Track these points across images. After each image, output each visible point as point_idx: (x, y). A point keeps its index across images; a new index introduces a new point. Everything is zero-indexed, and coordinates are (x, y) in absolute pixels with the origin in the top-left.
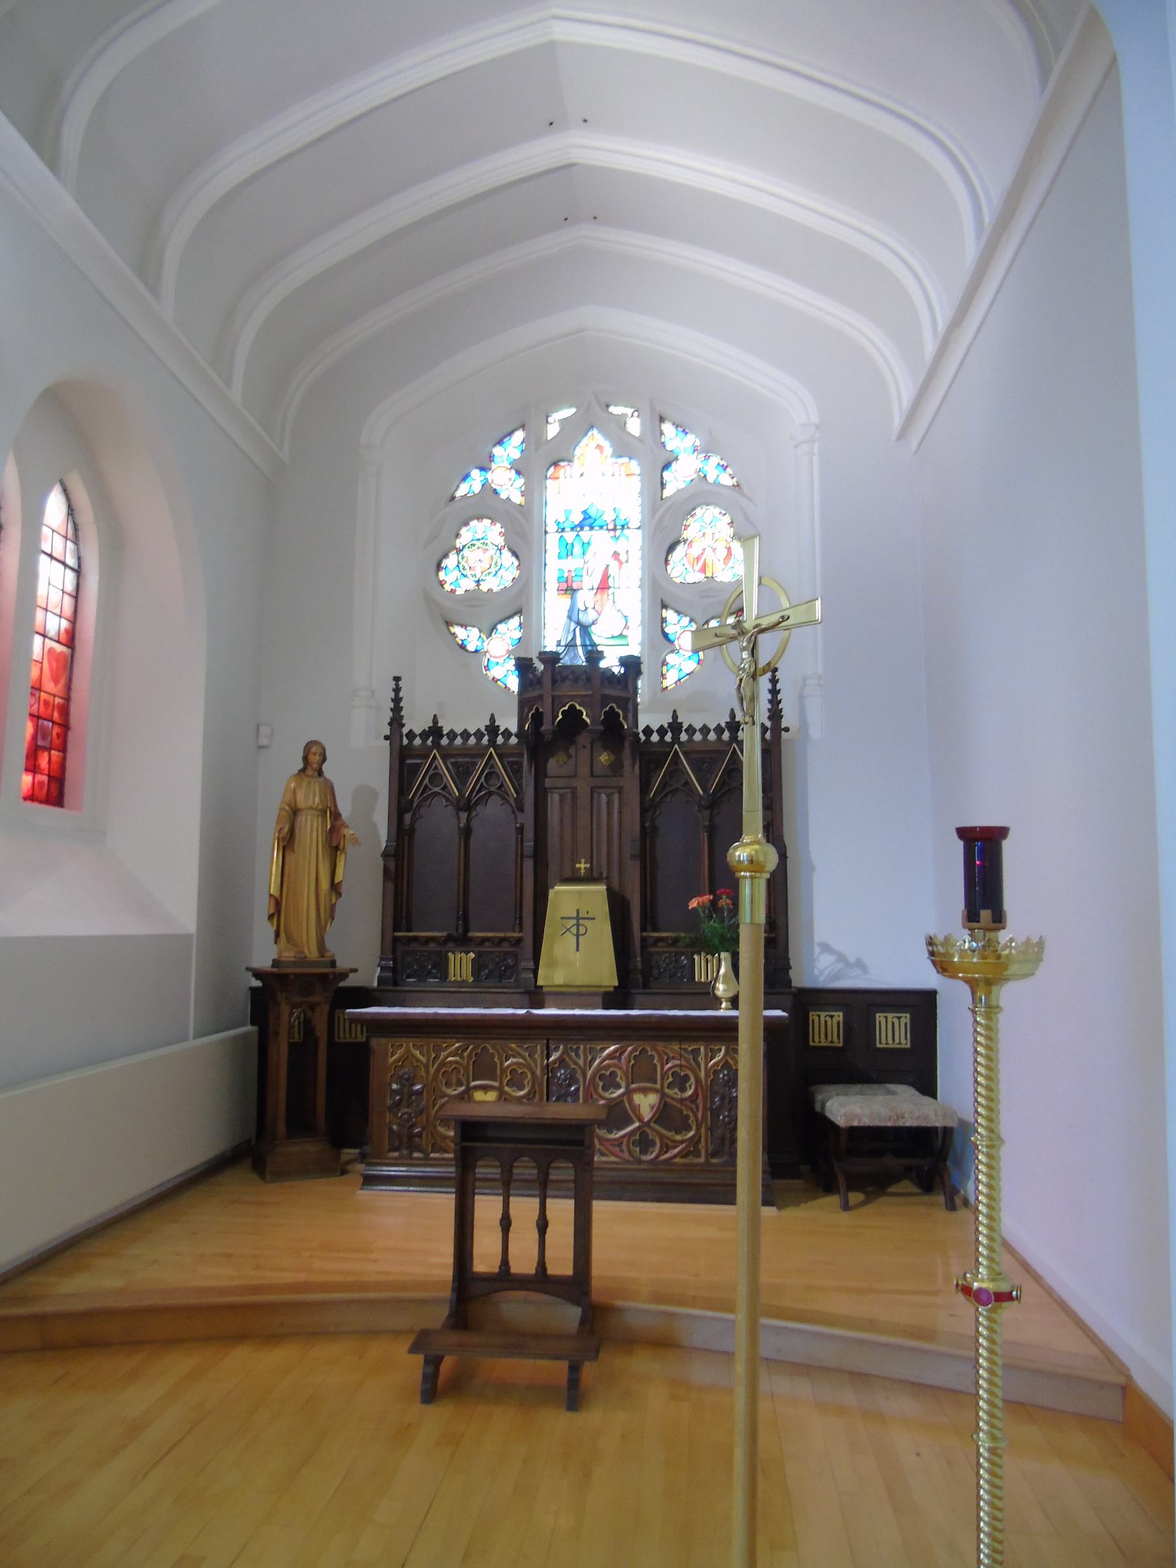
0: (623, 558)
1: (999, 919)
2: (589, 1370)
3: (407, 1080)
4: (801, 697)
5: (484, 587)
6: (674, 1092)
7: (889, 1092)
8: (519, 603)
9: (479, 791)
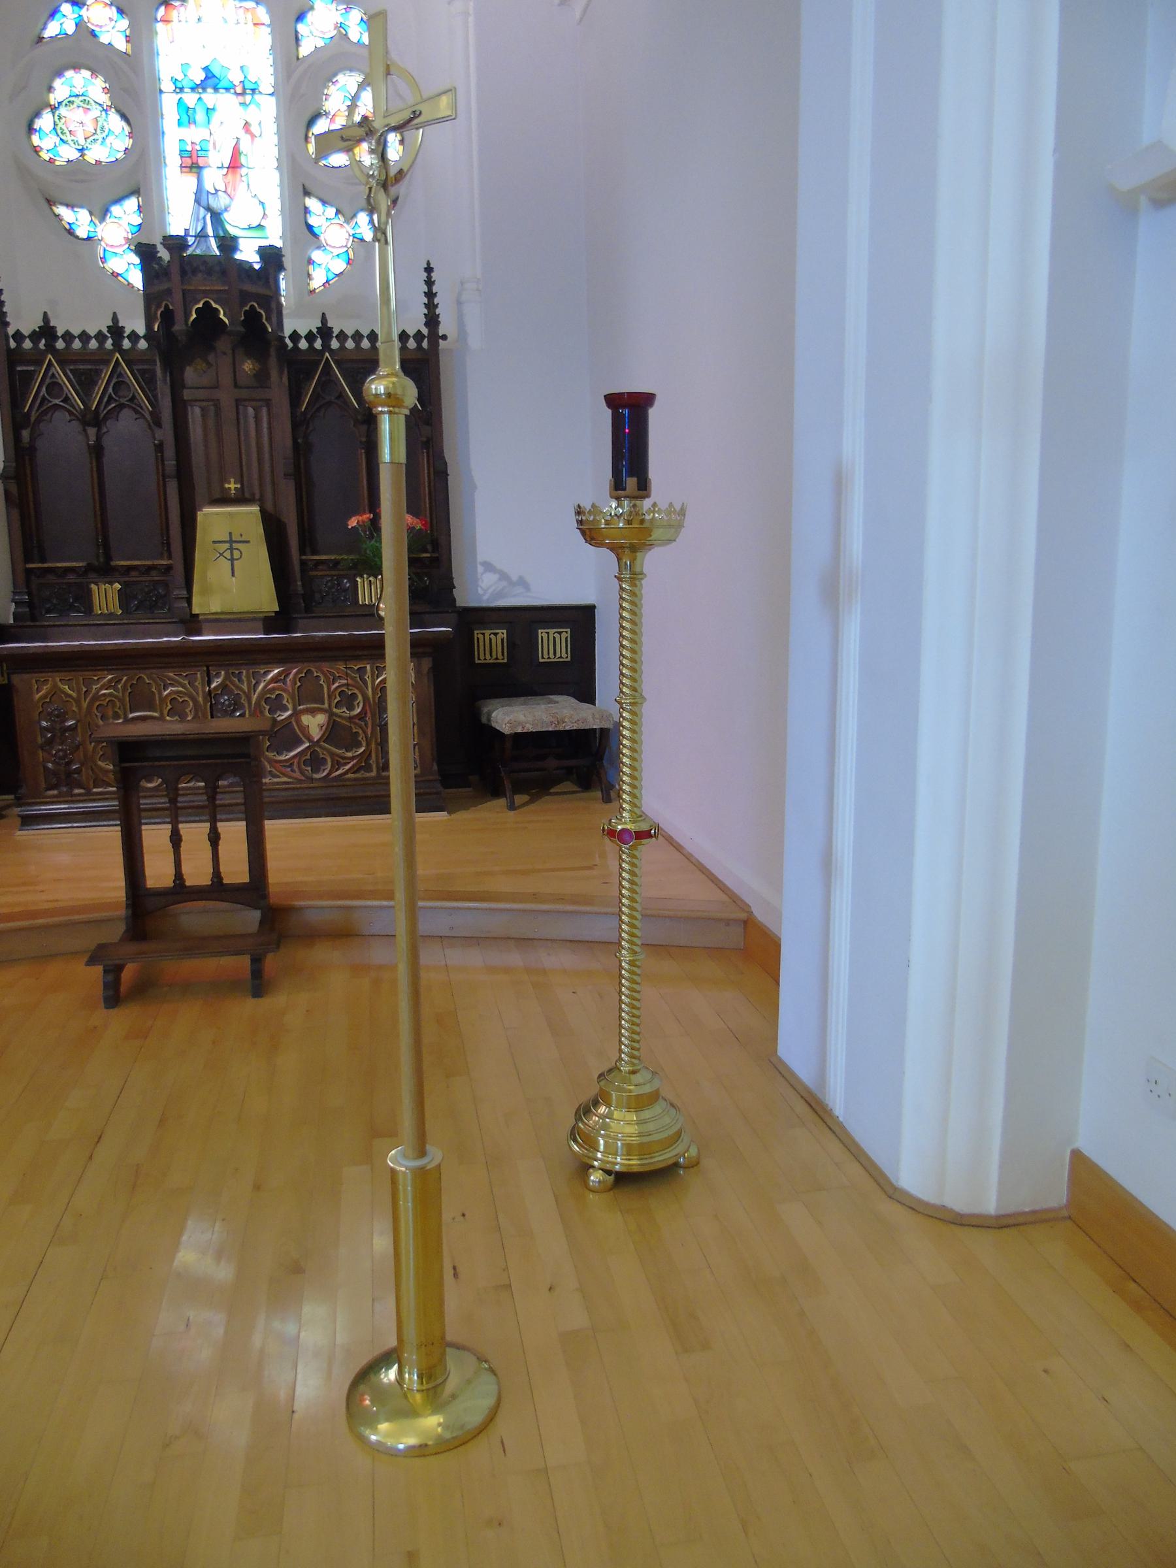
0: (254, 129)
1: (644, 486)
2: (271, 962)
3: (57, 716)
4: (459, 303)
5: (91, 157)
6: (343, 711)
7: (551, 702)
8: (135, 177)
9: (108, 403)
